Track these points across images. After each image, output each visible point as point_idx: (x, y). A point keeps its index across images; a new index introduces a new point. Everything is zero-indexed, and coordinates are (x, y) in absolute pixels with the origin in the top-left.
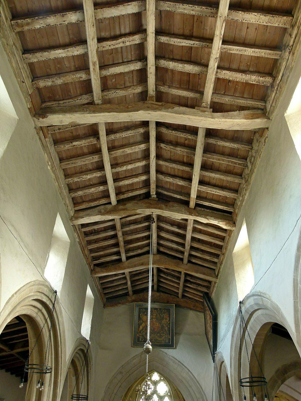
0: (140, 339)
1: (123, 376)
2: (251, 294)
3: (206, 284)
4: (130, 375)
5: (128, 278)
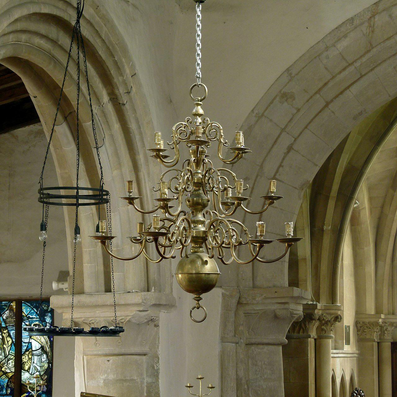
1: (298, 110)
4: (327, 104)
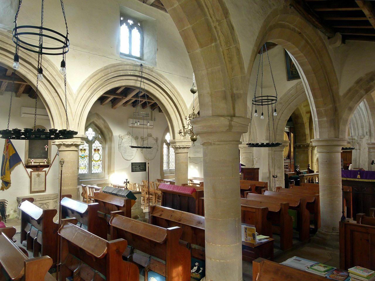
0: (294, 73)
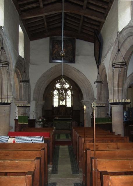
0: (54, 58)
2: (128, 26)
3: (97, 24)
5: (45, 20)
